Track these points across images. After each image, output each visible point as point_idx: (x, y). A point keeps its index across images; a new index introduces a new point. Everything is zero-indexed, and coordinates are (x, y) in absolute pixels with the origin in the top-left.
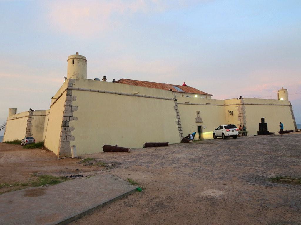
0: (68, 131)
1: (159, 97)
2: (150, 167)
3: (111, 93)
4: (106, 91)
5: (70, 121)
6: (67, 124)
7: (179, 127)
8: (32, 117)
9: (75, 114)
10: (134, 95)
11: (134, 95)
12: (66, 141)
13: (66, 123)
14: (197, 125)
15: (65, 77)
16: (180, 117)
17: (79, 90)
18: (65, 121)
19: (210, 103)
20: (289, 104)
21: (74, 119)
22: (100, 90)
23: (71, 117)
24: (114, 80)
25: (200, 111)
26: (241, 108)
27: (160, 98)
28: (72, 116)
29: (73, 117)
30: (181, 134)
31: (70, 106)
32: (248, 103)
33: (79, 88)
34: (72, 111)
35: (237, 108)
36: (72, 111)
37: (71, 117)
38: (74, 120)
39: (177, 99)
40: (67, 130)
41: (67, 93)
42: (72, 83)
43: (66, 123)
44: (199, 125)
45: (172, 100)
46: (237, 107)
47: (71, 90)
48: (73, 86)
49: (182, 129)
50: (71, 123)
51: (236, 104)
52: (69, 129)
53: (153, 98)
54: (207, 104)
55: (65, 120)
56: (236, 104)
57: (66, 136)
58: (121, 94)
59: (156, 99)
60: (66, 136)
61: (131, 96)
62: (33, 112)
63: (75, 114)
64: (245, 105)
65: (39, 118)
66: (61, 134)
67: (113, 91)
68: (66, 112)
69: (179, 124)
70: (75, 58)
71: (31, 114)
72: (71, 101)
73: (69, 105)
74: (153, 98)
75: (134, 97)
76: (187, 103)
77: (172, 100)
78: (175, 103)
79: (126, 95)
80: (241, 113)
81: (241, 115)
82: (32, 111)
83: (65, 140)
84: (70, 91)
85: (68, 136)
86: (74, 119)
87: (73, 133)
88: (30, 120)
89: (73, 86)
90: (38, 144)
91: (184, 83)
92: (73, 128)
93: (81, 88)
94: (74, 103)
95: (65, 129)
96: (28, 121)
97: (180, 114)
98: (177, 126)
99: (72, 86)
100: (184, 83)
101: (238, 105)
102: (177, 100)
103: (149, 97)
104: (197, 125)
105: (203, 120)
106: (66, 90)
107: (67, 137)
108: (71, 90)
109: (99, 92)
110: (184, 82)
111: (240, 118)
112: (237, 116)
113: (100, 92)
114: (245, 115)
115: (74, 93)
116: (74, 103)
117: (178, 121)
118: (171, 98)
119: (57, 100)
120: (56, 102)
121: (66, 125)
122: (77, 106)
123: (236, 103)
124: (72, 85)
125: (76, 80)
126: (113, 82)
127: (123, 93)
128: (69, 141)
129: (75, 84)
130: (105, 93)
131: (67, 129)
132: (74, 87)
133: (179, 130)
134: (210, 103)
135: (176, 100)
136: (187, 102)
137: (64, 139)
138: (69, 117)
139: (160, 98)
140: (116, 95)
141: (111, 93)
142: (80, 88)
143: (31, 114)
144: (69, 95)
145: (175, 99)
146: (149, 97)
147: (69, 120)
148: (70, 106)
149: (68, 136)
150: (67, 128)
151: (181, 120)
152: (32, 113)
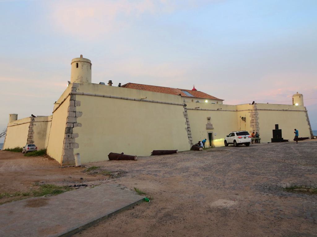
0: (71, 138)
1: (167, 102)
4: (112, 96)
5: (73, 127)
6: (71, 130)
7: (188, 134)
9: (79, 120)
10: (141, 100)
11: (141, 100)
14: (207, 132)
16: (190, 123)
18: (69, 128)
19: (221, 109)
21: (78, 125)
22: (105, 95)
23: (75, 123)
26: (254, 114)
28: (76, 123)
30: (191, 141)
31: (74, 112)
32: (261, 109)
33: (83, 93)
34: (76, 117)
36: (76, 117)
38: (78, 127)
39: (186, 104)
40: (70, 137)
41: (71, 98)
43: (69, 130)
44: (210, 131)
45: (181, 105)
46: (250, 112)
47: (75, 94)
49: (192, 136)
50: (75, 130)
51: (249, 110)
52: (73, 135)
53: (162, 103)
54: (218, 109)
55: (68, 127)
56: (249, 110)
57: (70, 143)
58: (127, 99)
61: (138, 101)
62: (35, 118)
63: (79, 120)
64: (258, 111)
67: (120, 96)
69: (188, 131)
70: (79, 61)
71: (33, 120)
72: (75, 106)
73: (73, 111)
74: (162, 103)
75: (141, 102)
76: (197, 109)
78: (185, 108)
79: (132, 100)
81: (254, 121)
83: (69, 148)
84: (74, 96)
85: (72, 143)
86: (78, 126)
87: (77, 140)
91: (194, 87)
92: (77, 135)
93: (85, 93)
94: (78, 109)
95: (69, 136)
97: (189, 120)
98: (186, 133)
99: (75, 91)
100: (194, 87)
101: (250, 111)
102: (186, 105)
103: (157, 102)
105: (214, 126)
106: (70, 94)
108: (75, 94)
109: (104, 97)
110: (194, 86)
111: (253, 124)
115: (78, 98)
116: (78, 109)
117: (188, 128)
118: (180, 103)
119: (60, 106)
122: (81, 112)
124: (76, 89)
126: (119, 86)
127: (129, 98)
128: (73, 149)
132: (78, 91)
133: (189, 137)
134: (221, 109)
135: (185, 105)
136: (197, 108)
137: (68, 147)
138: (73, 123)
143: (33, 120)
146: (157, 102)
147: (73, 127)
148: (74, 112)
149: (72, 143)
150: (70, 134)
152: (33, 119)
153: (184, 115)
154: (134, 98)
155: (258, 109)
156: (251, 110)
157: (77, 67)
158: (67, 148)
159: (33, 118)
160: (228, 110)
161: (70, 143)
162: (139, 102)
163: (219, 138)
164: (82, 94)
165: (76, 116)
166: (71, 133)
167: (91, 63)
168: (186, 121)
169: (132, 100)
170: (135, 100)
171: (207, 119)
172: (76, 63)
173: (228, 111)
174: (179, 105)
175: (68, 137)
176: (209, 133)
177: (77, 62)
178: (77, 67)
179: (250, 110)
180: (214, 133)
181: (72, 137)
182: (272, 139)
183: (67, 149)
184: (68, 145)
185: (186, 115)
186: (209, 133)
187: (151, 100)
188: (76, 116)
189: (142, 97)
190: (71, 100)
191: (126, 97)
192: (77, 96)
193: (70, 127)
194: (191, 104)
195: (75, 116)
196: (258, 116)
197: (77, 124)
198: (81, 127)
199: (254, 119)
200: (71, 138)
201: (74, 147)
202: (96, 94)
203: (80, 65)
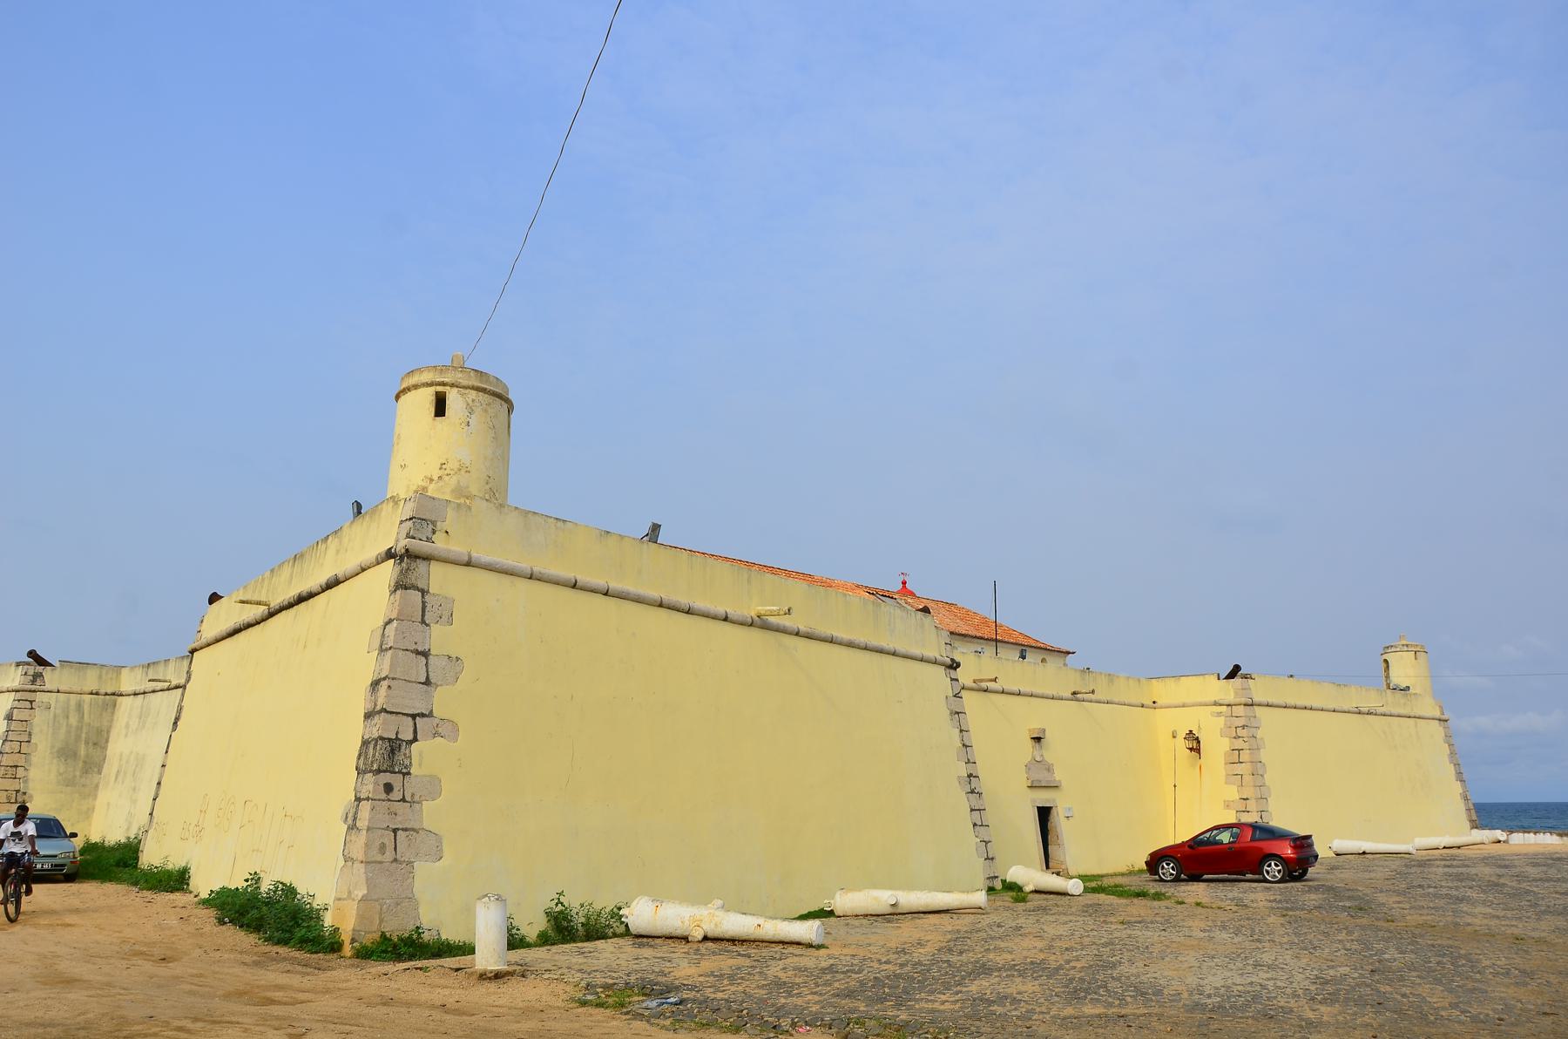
0: (403, 800)
1: (874, 642)
2: (576, 1001)
3: (639, 600)
4: (615, 585)
5: (415, 739)
6: (399, 757)
7: (972, 810)
8: (40, 698)
9: (443, 701)
10: (760, 624)
11: (760, 624)
12: (395, 860)
13: (392, 751)
14: (1033, 801)
16: (978, 753)
17: (468, 564)
18: (390, 740)
19: (1093, 692)
21: (441, 731)
22: (583, 578)
23: (423, 715)
24: (656, 528)
25: (1044, 731)
26: (1241, 722)
27: (880, 651)
28: (430, 715)
29: (437, 721)
30: (986, 843)
31: (418, 653)
32: (1271, 700)
33: (470, 558)
34: (427, 682)
35: (1222, 720)
36: (427, 682)
37: (423, 715)
39: (957, 659)
40: (396, 795)
41: (404, 573)
42: (434, 523)
43: (392, 751)
44: (1043, 798)
45: (935, 662)
46: (1219, 714)
47: (427, 558)
48: (434, 538)
49: (989, 817)
50: (425, 756)
51: (1216, 704)
52: (412, 786)
53: (850, 645)
54: (1074, 693)
55: (385, 735)
56: (1216, 704)
58: (689, 612)
60: (395, 831)
61: (742, 624)
62: (47, 672)
63: (443, 701)
64: (1437, 714)
65: (79, 706)
67: (653, 593)
68: (392, 683)
69: (972, 792)
71: (33, 682)
72: (423, 622)
73: (413, 647)
74: (850, 645)
75: (755, 634)
76: (984, 685)
77: (935, 662)
78: (952, 679)
79: (715, 617)
80: (1239, 744)
81: (1245, 756)
82: (41, 661)
83: (389, 855)
84: (422, 565)
85: (405, 830)
86: (436, 734)
87: (431, 814)
88: (24, 715)
89: (434, 538)
90: (646, 895)
91: (904, 583)
92: (434, 787)
93: (480, 555)
94: (439, 639)
95: (388, 788)
96: (9, 718)
97: (975, 738)
98: (963, 802)
99: (429, 540)
100: (904, 583)
101: (1224, 708)
102: (958, 665)
103: (831, 641)
104: (1033, 801)
105: (1058, 775)
106: (390, 554)
107: (399, 833)
108: (427, 558)
110: (902, 578)
111: (1239, 769)
112: (1220, 761)
113: (583, 589)
114: (1264, 755)
115: (439, 578)
116: (439, 639)
117: (970, 776)
118: (931, 653)
119: (271, 615)
120: (258, 623)
121: (392, 766)
122: (458, 659)
123: (1212, 699)
124: (434, 532)
125: (459, 505)
127: (699, 604)
128: (410, 863)
129: (446, 526)
130: (606, 594)
131: (397, 786)
132: (440, 544)
133: (975, 825)
134: (1093, 692)
135: (954, 665)
136: (982, 681)
137: (383, 847)
138: (414, 716)
139: (880, 651)
140: (663, 612)
141: (639, 600)
142: (474, 555)
143: (33, 682)
145: (948, 661)
146: (831, 641)
147: (410, 737)
148: (418, 653)
149: (405, 830)
150: (395, 780)
151: (981, 769)
152: (37, 677)
153: (951, 713)
154: (721, 610)
155: (1257, 699)
156: (1228, 705)
157: (440, 408)
158: (379, 858)
159: (40, 669)
160: (1116, 700)
161: (395, 831)
164: (466, 558)
165: (427, 678)
166: (400, 772)
167: (510, 397)
168: (961, 745)
169: (715, 617)
170: (726, 619)
171: (1028, 738)
172: (432, 390)
173: (1118, 704)
174: (928, 661)
175: (384, 796)
176: (1039, 809)
177: (440, 389)
179: (1221, 705)
180: (1060, 810)
181: (408, 798)
182: (224, 892)
183: (381, 862)
184: (386, 841)
185: (958, 713)
186: (1054, 812)
187: (803, 628)
188: (427, 678)
189: (762, 609)
190: (400, 585)
191: (683, 600)
192: (435, 567)
193: (397, 739)
194: (975, 666)
195: (423, 680)
196: (1259, 734)
197: (436, 721)
199: (1245, 746)
202: (536, 569)
203: (454, 399)
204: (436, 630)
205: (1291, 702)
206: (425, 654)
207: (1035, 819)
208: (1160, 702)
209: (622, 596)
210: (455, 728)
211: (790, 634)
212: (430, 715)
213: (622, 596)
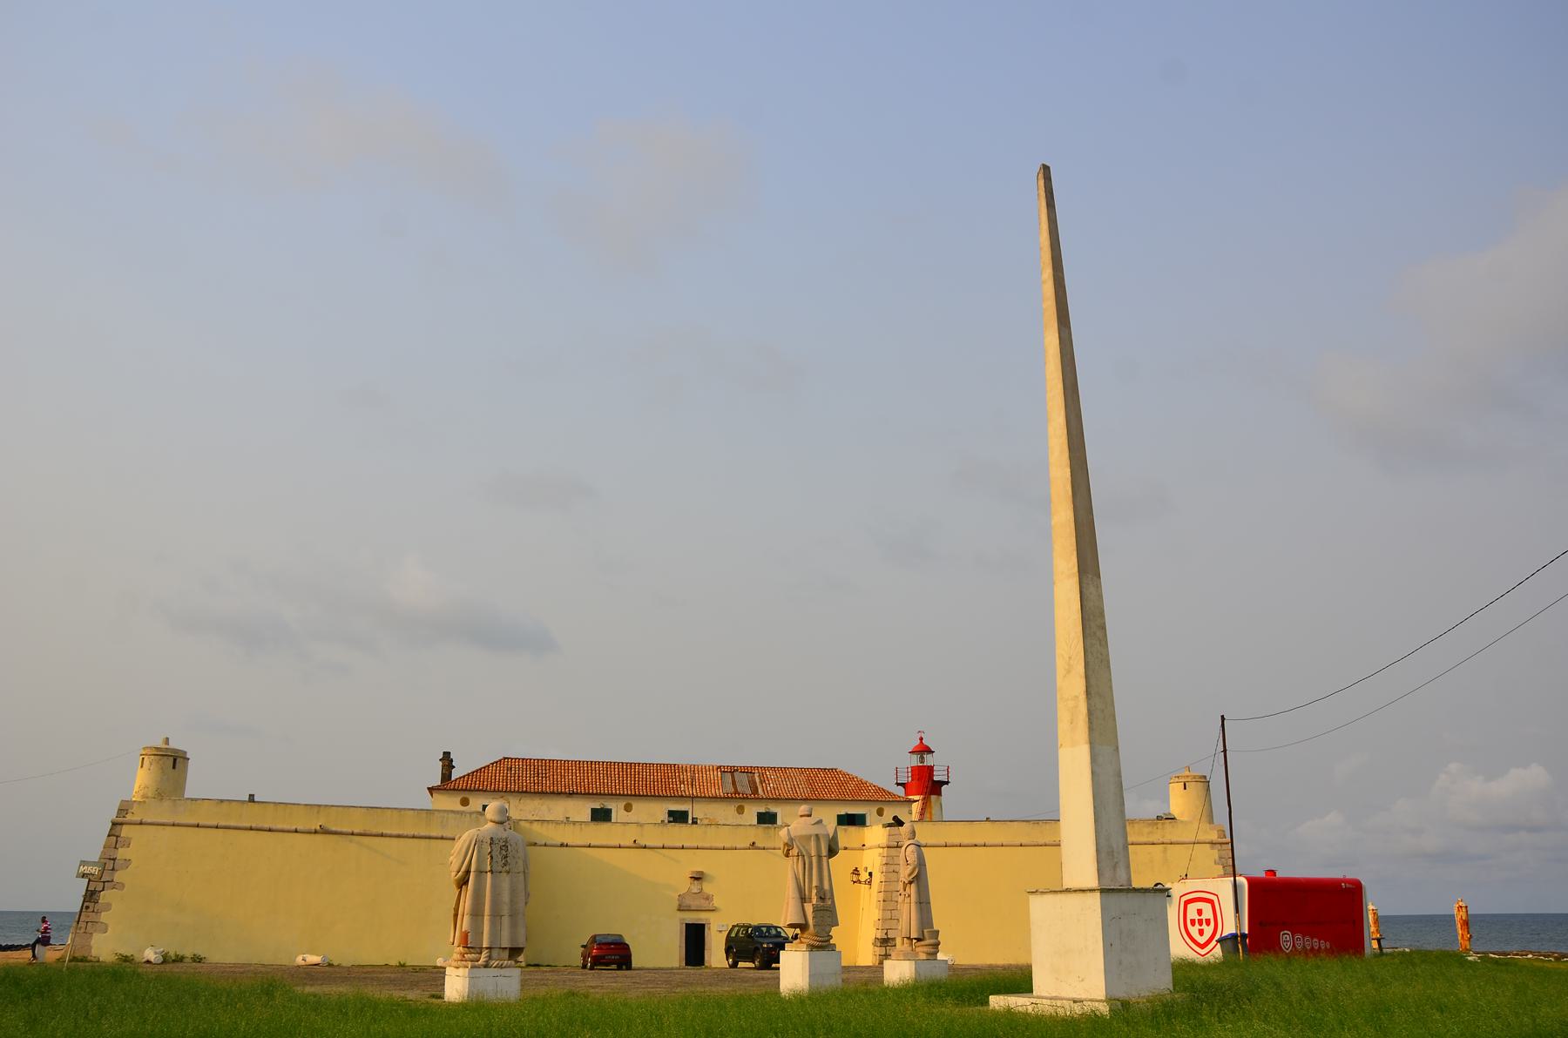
0: (93, 911)
5: (103, 890)
6: (94, 897)
9: (118, 877)
11: (324, 831)
15: (447, 755)
17: (141, 824)
20: (115, 868)
28: (112, 881)
36: (113, 869)
38: (114, 890)
42: (127, 810)
44: (692, 918)
57: (87, 922)
59: (411, 840)
66: (859, 975)
70: (146, 755)
79: (957, 846)
84: (119, 827)
91: (921, 739)
92: (108, 907)
99: (124, 817)
100: (921, 739)
104: (681, 920)
105: (716, 903)
108: (122, 824)
109: (198, 826)
116: (121, 853)
126: (447, 783)
132: (129, 817)
144: (114, 835)
150: (91, 905)
157: (1185, 788)
161: (87, 922)
162: (313, 835)
163: (1009, 1011)
170: (296, 831)
178: (1185, 788)
198: (123, 889)
200: (93, 911)
201: (95, 931)
204: (120, 850)
205: (966, 841)
206: (114, 859)
207: (681, 932)
208: (757, 845)
209: (179, 825)
210: (123, 885)
211: (266, 831)
212: (112, 881)
213: (179, 825)
